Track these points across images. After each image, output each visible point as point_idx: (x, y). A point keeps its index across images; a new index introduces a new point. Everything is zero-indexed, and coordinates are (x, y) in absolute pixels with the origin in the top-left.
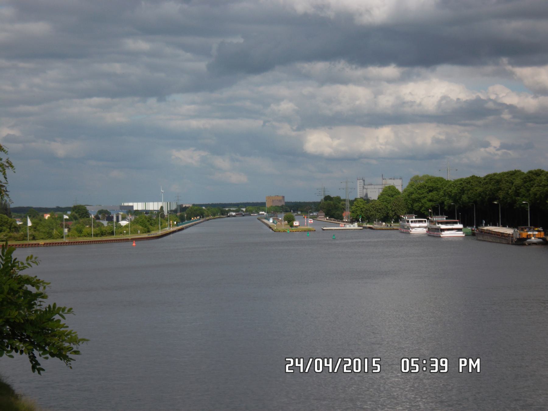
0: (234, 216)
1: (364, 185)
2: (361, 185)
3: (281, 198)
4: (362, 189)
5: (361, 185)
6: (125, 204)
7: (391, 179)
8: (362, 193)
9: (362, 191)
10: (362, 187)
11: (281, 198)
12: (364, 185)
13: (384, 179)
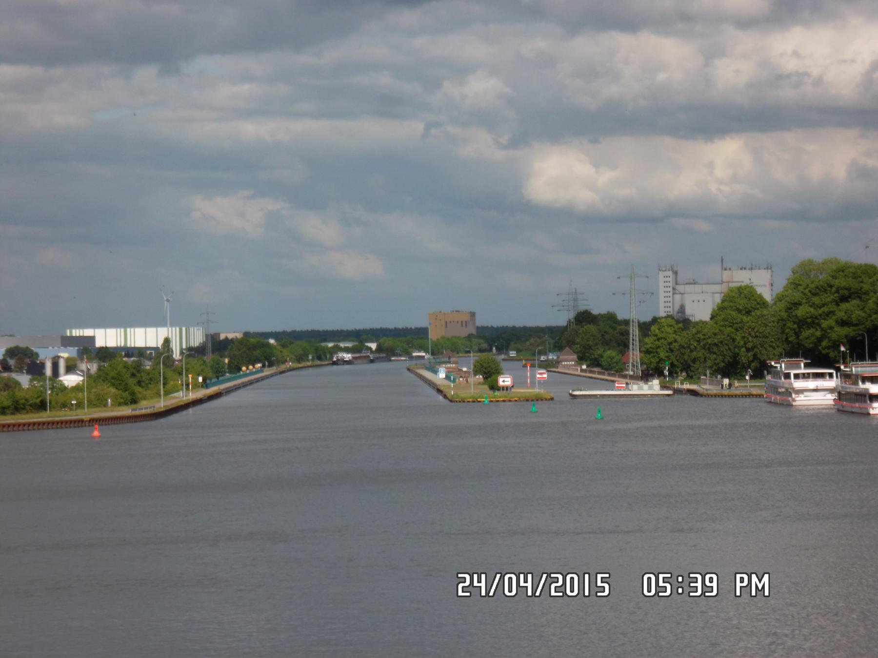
0: (349, 362)
1: (677, 284)
2: (668, 284)
3: (467, 318)
4: (671, 294)
5: (668, 284)
6: (74, 331)
7: (745, 269)
8: (671, 305)
9: (671, 299)
10: (671, 289)
11: (467, 318)
12: (677, 284)
13: (725, 269)
